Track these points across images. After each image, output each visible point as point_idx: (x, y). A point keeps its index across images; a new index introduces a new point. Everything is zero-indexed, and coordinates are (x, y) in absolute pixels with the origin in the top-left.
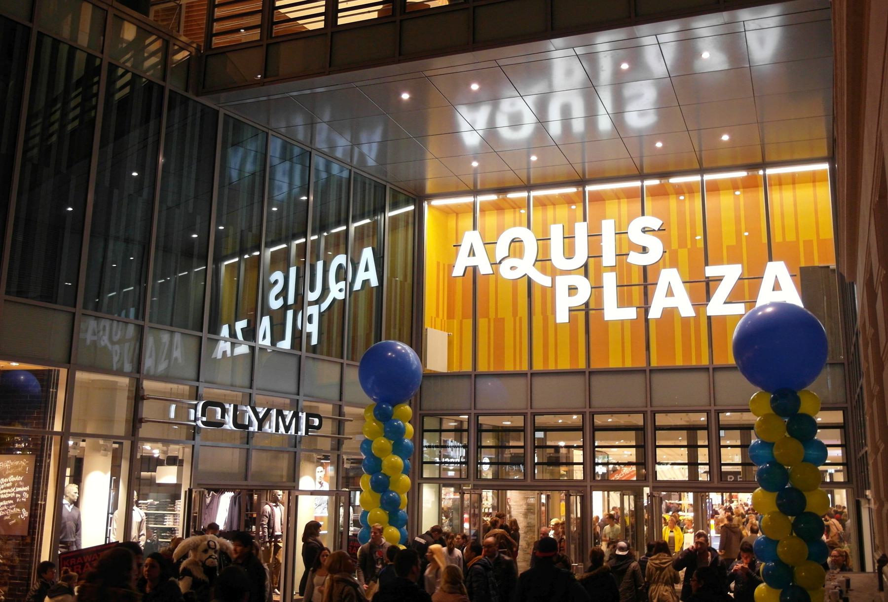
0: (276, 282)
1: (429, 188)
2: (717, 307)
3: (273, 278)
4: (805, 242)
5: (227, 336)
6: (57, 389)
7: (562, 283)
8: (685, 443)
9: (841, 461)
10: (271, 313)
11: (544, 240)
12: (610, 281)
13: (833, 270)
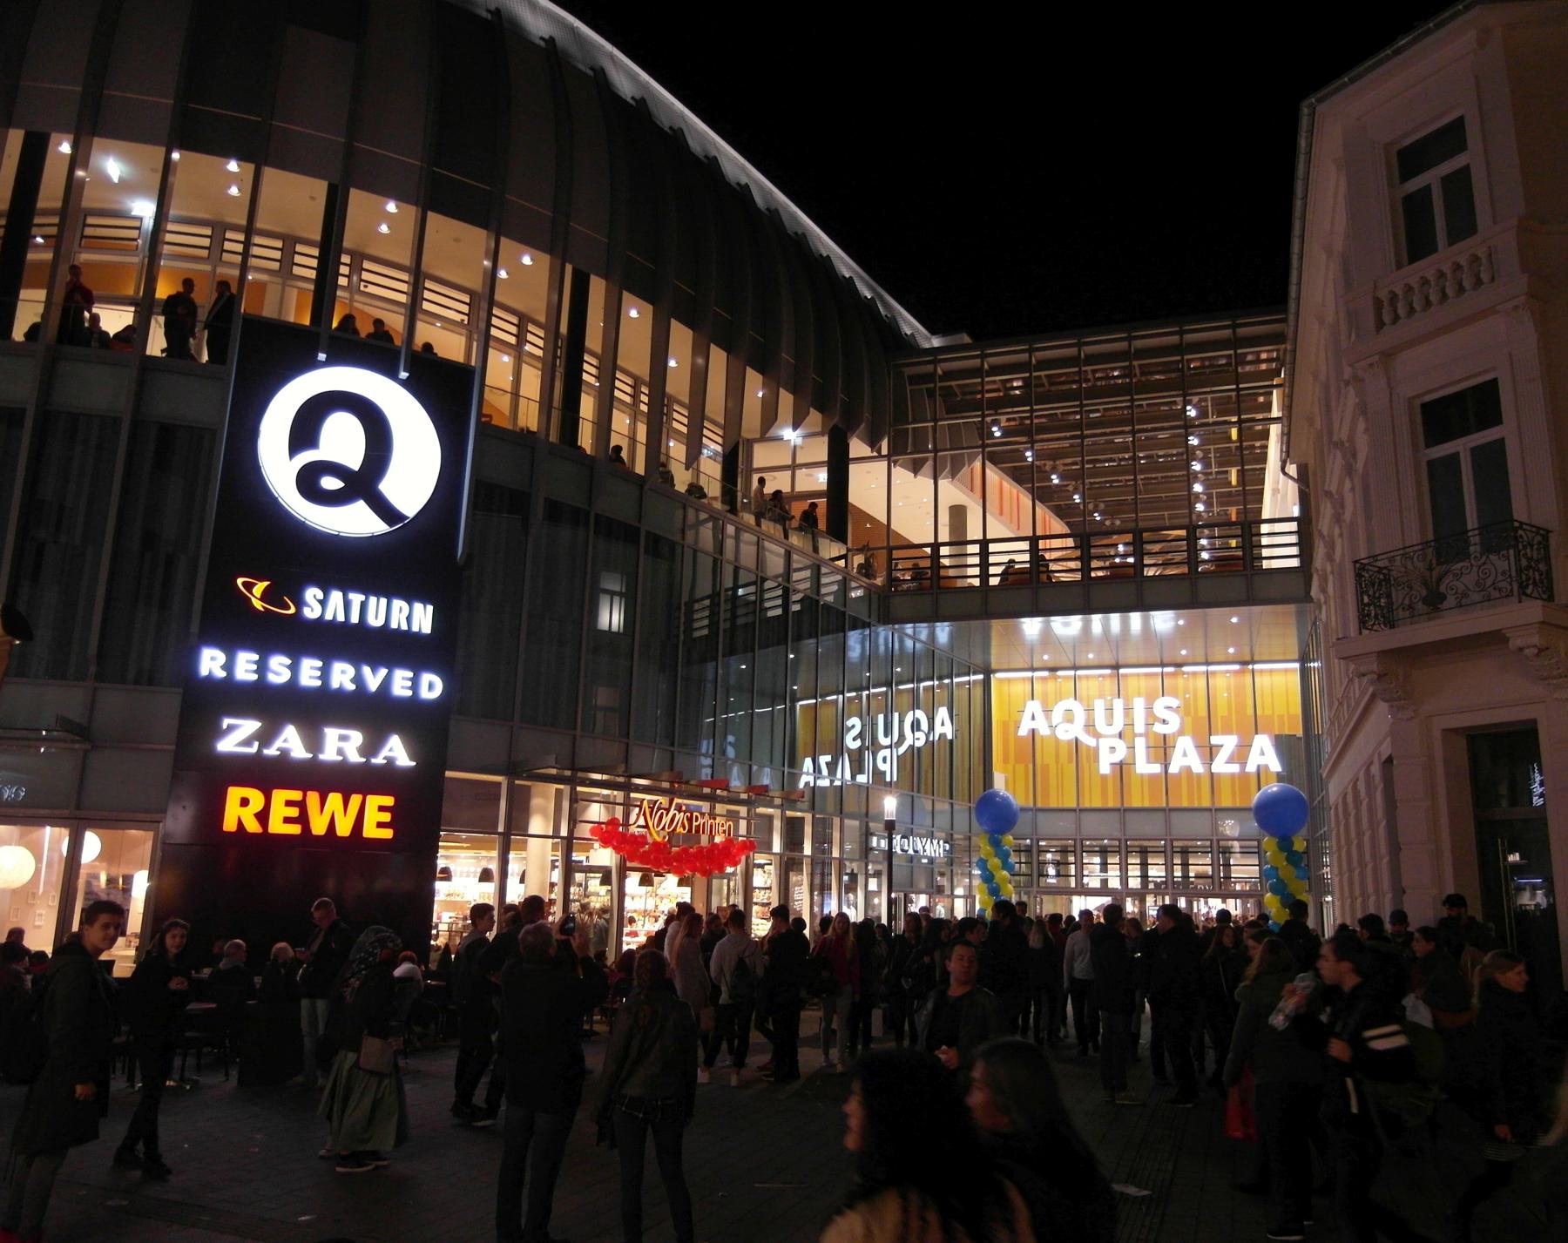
0: (853, 726)
1: (994, 666)
2: (1221, 766)
3: (849, 723)
4: (1279, 716)
5: (811, 771)
6: (832, 829)
7: (1104, 745)
8: (1180, 862)
9: (1190, 854)
10: (850, 752)
11: (1089, 710)
12: (1140, 744)
13: (1300, 739)
